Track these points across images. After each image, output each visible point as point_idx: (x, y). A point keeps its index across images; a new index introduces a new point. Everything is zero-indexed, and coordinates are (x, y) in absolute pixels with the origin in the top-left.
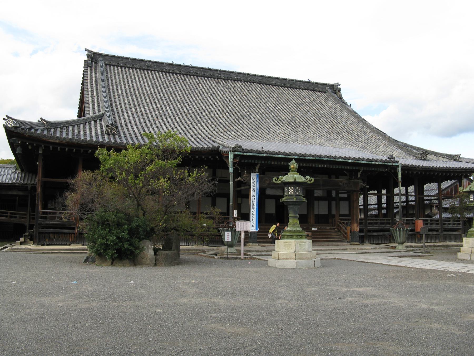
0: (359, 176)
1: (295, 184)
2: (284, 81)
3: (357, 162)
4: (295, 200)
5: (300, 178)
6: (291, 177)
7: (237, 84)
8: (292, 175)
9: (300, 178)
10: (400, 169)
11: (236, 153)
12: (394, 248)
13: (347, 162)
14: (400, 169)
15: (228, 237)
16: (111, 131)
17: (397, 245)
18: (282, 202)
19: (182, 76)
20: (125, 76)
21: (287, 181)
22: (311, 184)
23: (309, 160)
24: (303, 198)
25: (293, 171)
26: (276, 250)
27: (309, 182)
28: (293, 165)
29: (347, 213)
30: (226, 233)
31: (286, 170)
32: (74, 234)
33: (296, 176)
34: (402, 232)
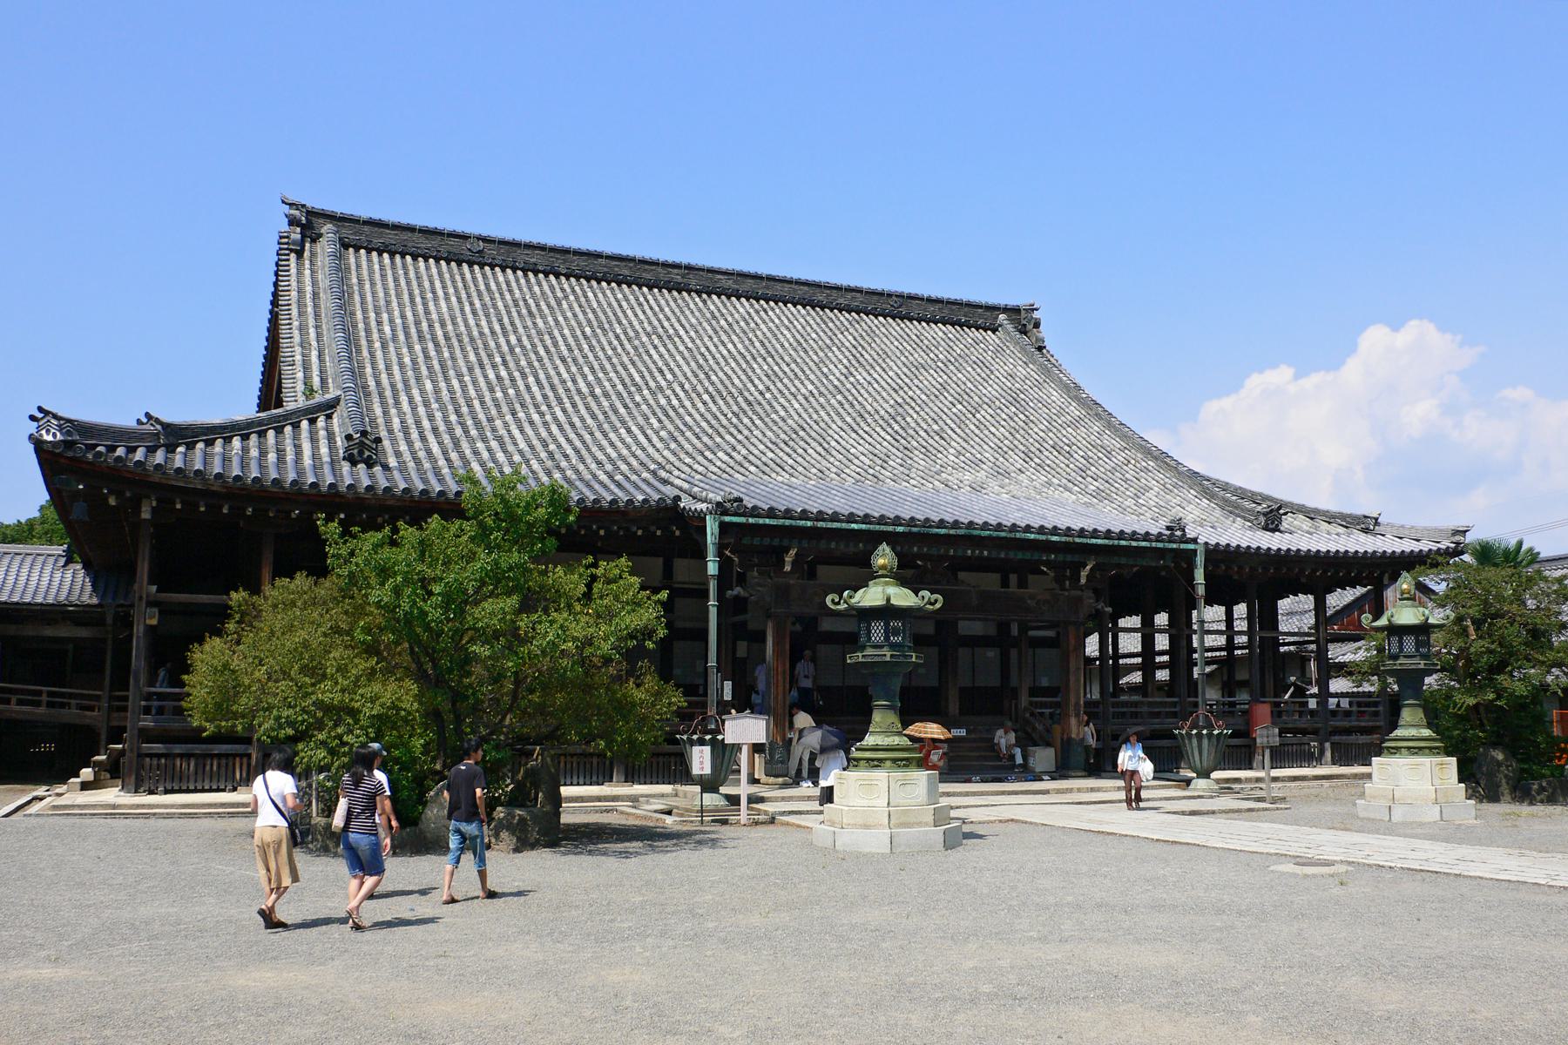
0: (1083, 581)
5: (903, 597)
10: (1200, 560)
11: (727, 519)
14: (1200, 560)
16: (361, 453)
23: (937, 535)
34: (1205, 742)
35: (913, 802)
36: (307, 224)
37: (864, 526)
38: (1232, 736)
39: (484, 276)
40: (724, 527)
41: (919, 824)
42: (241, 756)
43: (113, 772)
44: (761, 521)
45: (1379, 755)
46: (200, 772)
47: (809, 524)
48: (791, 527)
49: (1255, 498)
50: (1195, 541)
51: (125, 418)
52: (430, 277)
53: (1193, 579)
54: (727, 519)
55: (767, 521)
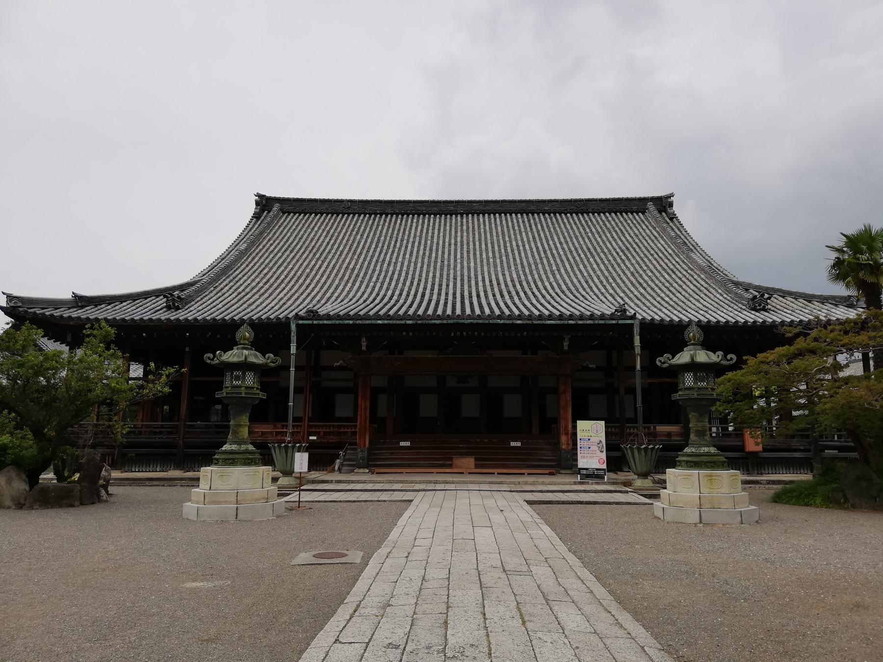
0: (566, 348)
1: (245, 366)
2: (566, 204)
3: (580, 322)
4: (243, 395)
5: (256, 358)
6: (233, 356)
7: (637, 217)
8: (240, 351)
9: (256, 358)
10: (636, 330)
11: (301, 322)
12: (627, 484)
13: (406, 325)
14: (636, 330)
15: (301, 464)
16: (174, 304)
17: (631, 476)
18: (677, 401)
19: (613, 214)
20: (493, 225)
21: (231, 360)
22: (210, 365)
23: (435, 324)
24: (258, 392)
25: (693, 344)
26: (668, 487)
27: (272, 365)
28: (246, 333)
29: (350, 414)
30: (298, 455)
31: (678, 346)
32: (113, 455)
33: (246, 352)
34: (636, 452)
35: (227, 487)
36: (264, 203)
37: (559, 322)
38: (661, 450)
39: (546, 219)
40: (298, 325)
41: (226, 502)
42: (109, 455)
43: (353, 465)
44: (321, 322)
45: (674, 466)
46: (708, 467)
47: (351, 322)
48: (340, 324)
49: (747, 287)
50: (633, 317)
51: (66, 295)
52: (621, 222)
53: (633, 343)
54: (301, 322)
55: (325, 322)
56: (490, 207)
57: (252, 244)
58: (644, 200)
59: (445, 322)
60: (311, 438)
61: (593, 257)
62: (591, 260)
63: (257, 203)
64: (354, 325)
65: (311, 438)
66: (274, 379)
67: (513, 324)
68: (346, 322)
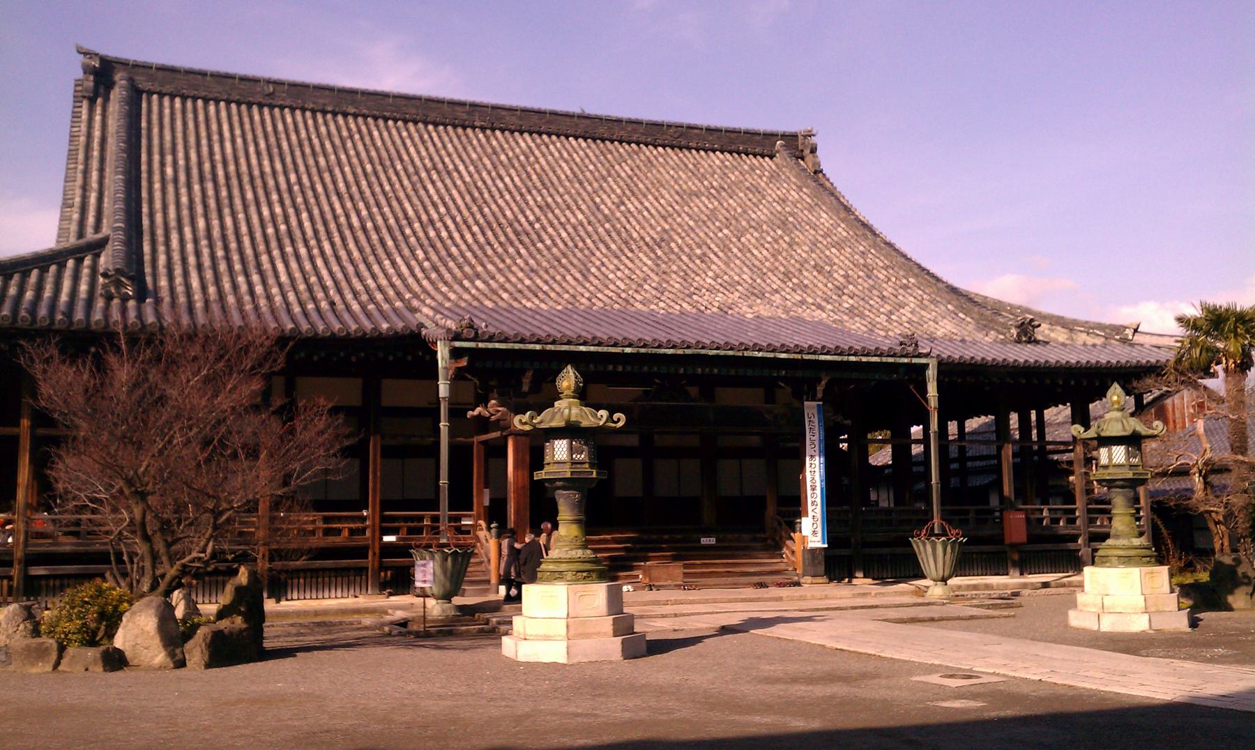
10: (931, 373)
11: (458, 344)
14: (931, 373)
23: (665, 355)
48: (520, 350)
56: (513, 121)
57: (842, 204)
58: (771, 136)
59: (680, 352)
60: (387, 539)
61: (380, 263)
62: (376, 268)
63: (87, 70)
64: (543, 352)
65: (387, 539)
66: (820, 389)
67: (775, 359)
68: (531, 347)
